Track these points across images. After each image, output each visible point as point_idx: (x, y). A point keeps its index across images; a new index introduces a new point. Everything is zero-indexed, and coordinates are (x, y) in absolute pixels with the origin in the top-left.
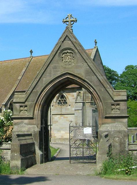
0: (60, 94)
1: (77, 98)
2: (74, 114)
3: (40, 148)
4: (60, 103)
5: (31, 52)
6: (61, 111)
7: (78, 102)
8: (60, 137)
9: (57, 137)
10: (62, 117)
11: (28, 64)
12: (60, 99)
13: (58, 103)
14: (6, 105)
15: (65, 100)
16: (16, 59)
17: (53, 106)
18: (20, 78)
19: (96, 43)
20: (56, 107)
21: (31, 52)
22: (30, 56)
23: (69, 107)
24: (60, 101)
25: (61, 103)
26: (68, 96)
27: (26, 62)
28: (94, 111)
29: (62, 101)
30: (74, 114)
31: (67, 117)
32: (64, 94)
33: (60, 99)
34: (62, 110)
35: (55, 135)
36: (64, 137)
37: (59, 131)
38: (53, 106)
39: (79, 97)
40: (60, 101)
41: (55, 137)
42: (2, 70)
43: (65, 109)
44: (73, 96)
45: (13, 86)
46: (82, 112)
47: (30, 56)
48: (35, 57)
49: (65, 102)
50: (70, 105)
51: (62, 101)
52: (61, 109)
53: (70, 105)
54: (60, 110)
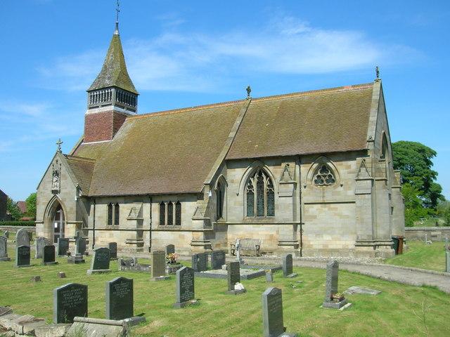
0: (320, 164)
1: (360, 171)
2: (354, 202)
3: (347, 255)
4: (319, 181)
5: (249, 90)
6: (323, 197)
7: (362, 178)
8: (321, 247)
9: (314, 247)
10: (325, 208)
11: (244, 110)
12: (319, 174)
13: (316, 181)
14: (211, 185)
15: (330, 176)
16: (218, 104)
17: (305, 187)
18: (232, 135)
19: (378, 72)
20: (312, 188)
21: (249, 90)
22: (247, 97)
23: (340, 189)
24: (319, 177)
25: (323, 181)
26: (338, 167)
27: (240, 108)
28: (219, 257)
29: (323, 178)
30: (354, 202)
31: (336, 209)
32: (329, 164)
33: (319, 174)
34: (326, 194)
35: (311, 243)
36: (331, 247)
37: (319, 234)
38: (305, 187)
39: (363, 170)
40: (319, 177)
41: (310, 246)
42: (193, 123)
43: (330, 193)
44: (349, 167)
45: (220, 150)
46: (372, 199)
47: (247, 97)
48: (256, 99)
49: (331, 180)
50: (342, 186)
51: (323, 178)
52: (324, 193)
53: (342, 186)
54: (321, 195)
